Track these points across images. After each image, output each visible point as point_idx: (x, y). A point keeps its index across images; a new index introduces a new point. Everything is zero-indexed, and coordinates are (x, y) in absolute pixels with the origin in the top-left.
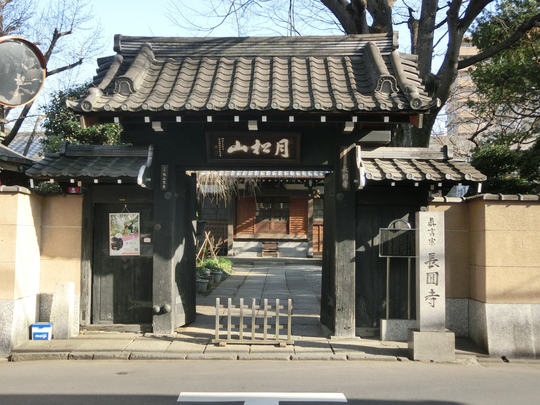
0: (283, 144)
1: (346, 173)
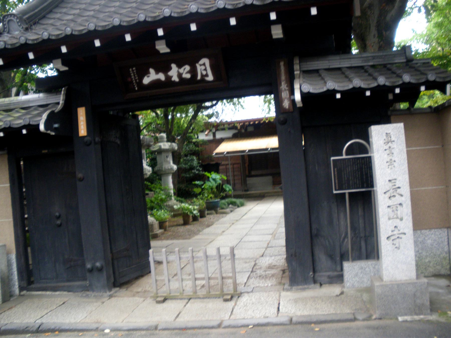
0: (204, 64)
1: (285, 90)
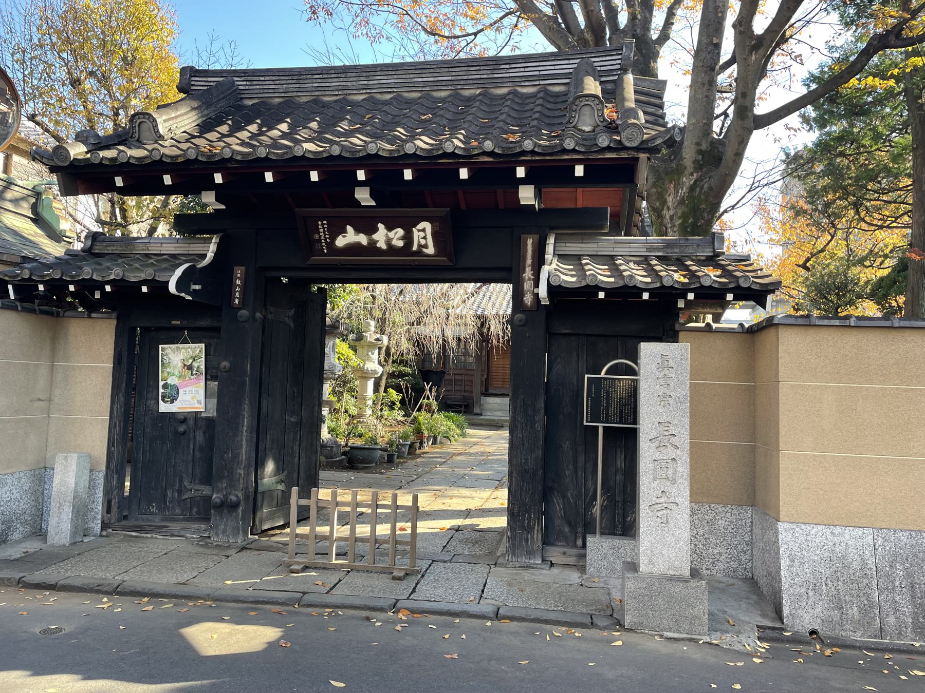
0: (424, 230)
1: (529, 279)
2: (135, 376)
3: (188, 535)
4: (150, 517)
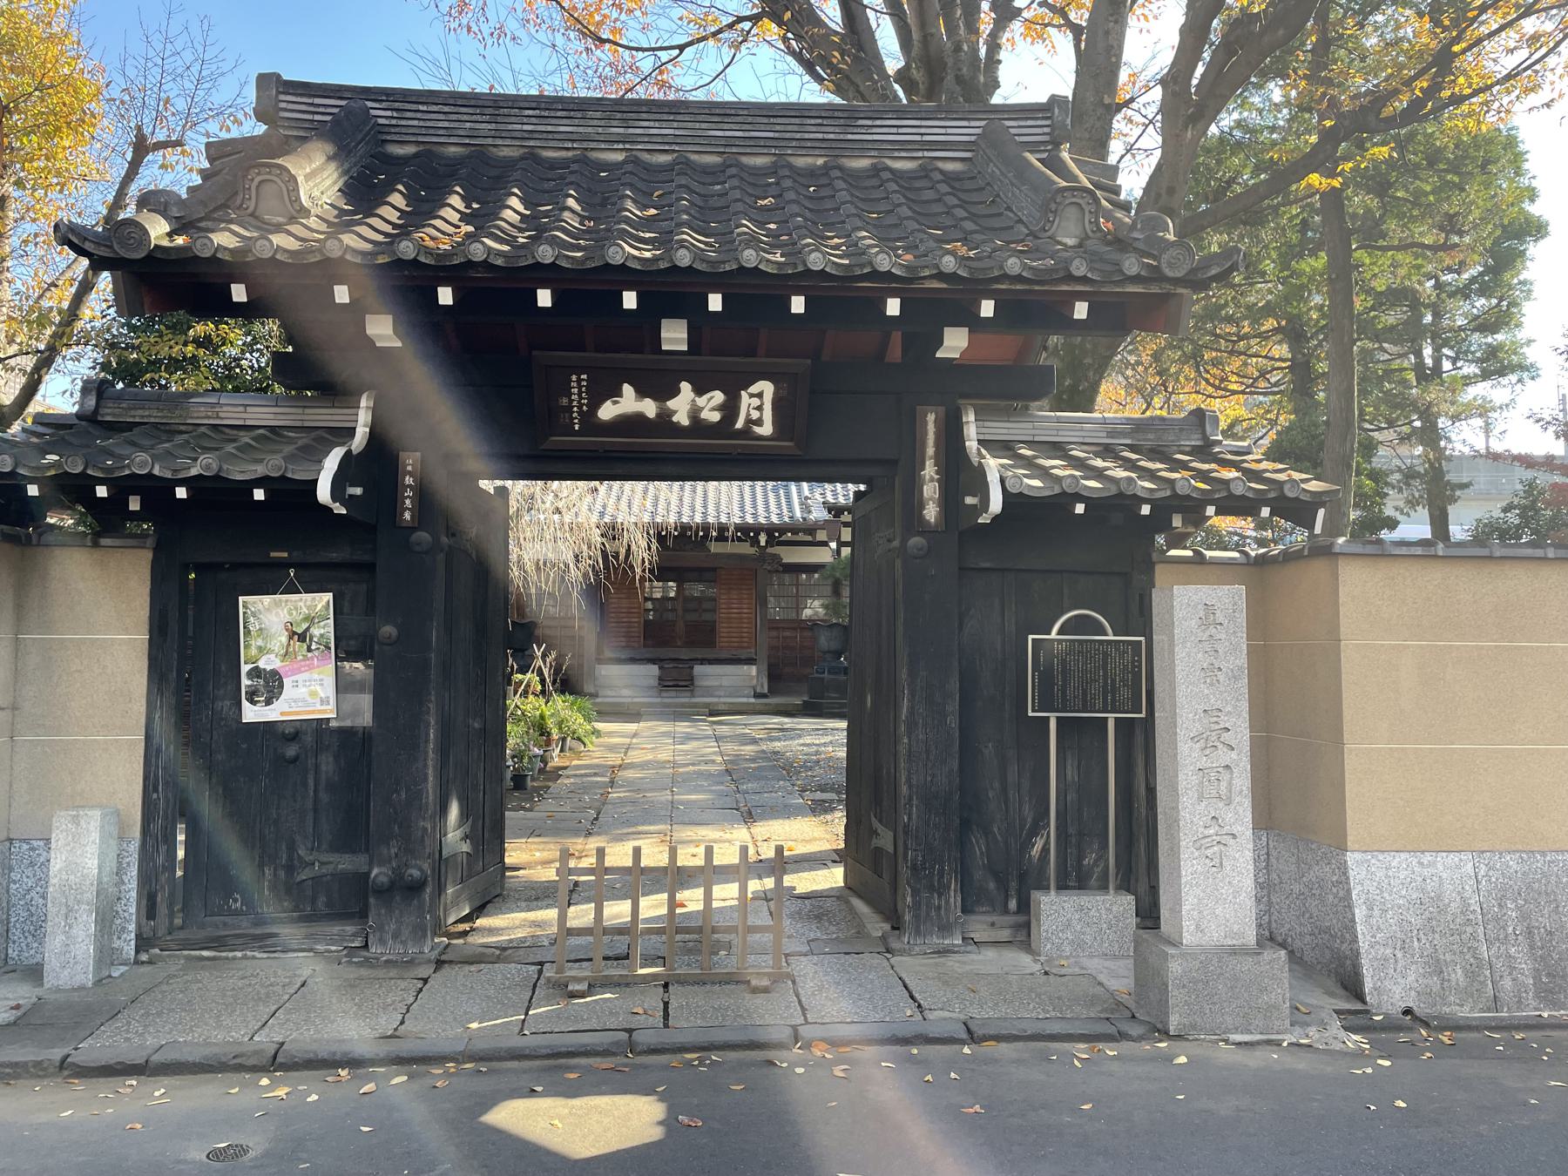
0: (760, 395)
1: (932, 480)
2: (193, 658)
3: (319, 947)
4: (227, 919)
